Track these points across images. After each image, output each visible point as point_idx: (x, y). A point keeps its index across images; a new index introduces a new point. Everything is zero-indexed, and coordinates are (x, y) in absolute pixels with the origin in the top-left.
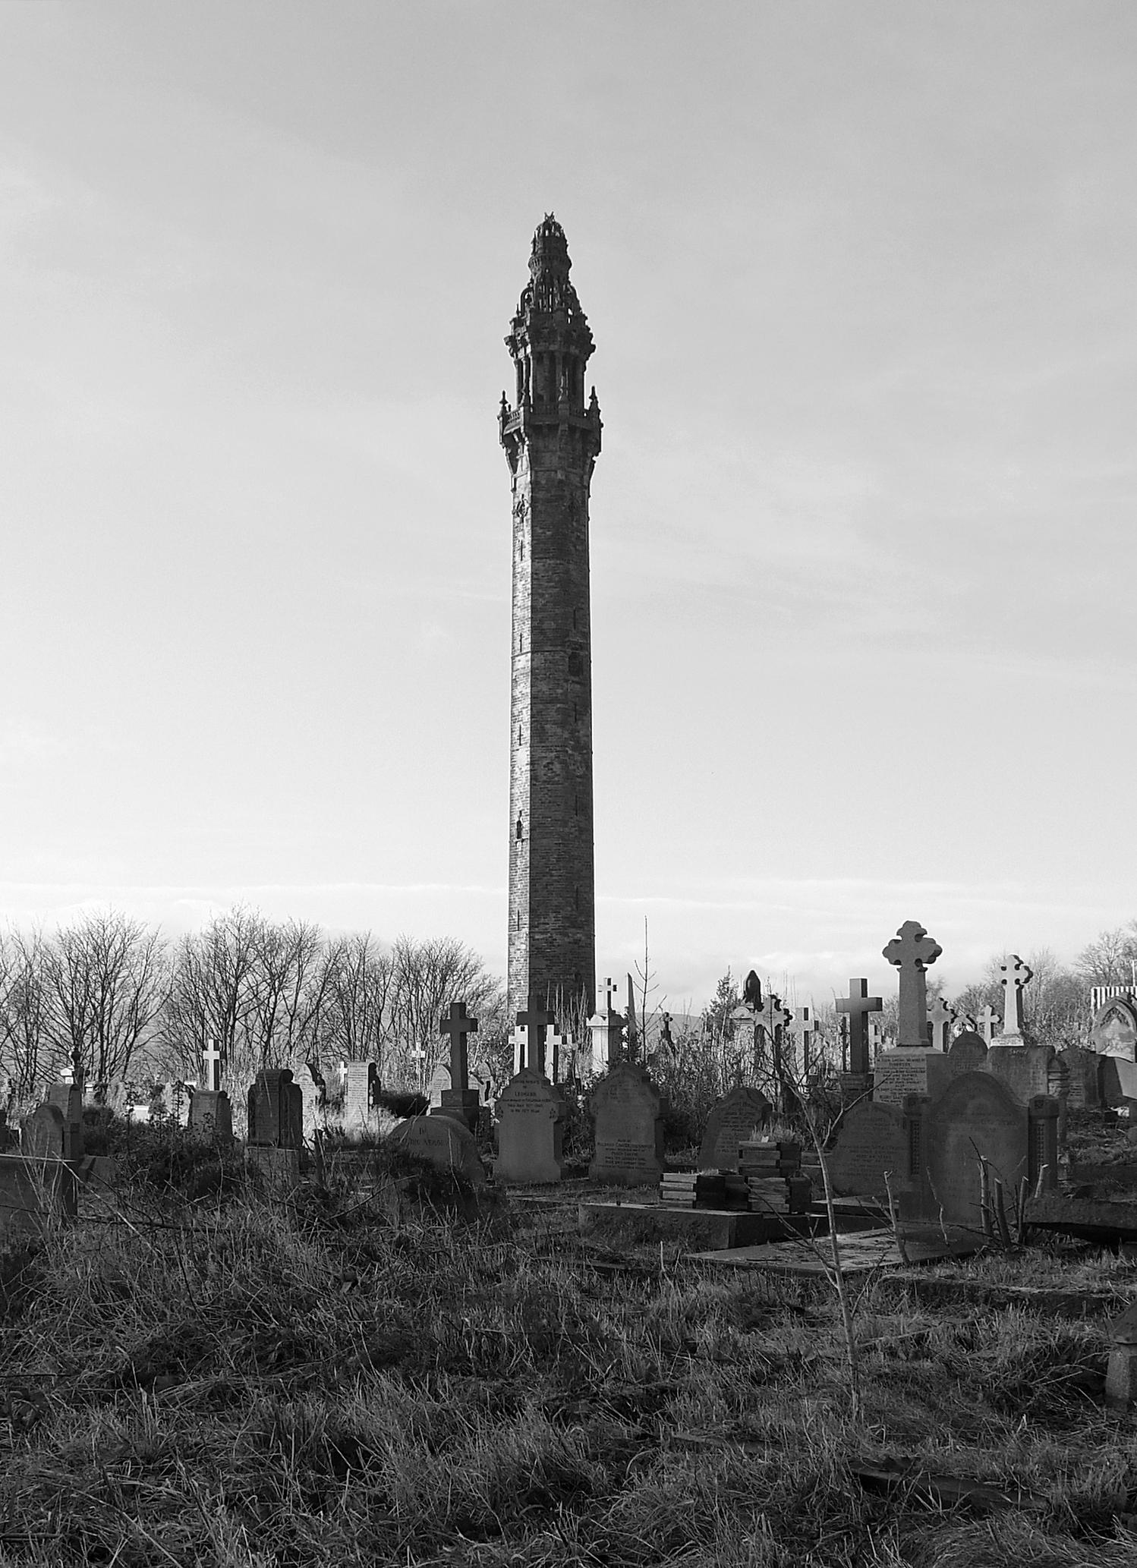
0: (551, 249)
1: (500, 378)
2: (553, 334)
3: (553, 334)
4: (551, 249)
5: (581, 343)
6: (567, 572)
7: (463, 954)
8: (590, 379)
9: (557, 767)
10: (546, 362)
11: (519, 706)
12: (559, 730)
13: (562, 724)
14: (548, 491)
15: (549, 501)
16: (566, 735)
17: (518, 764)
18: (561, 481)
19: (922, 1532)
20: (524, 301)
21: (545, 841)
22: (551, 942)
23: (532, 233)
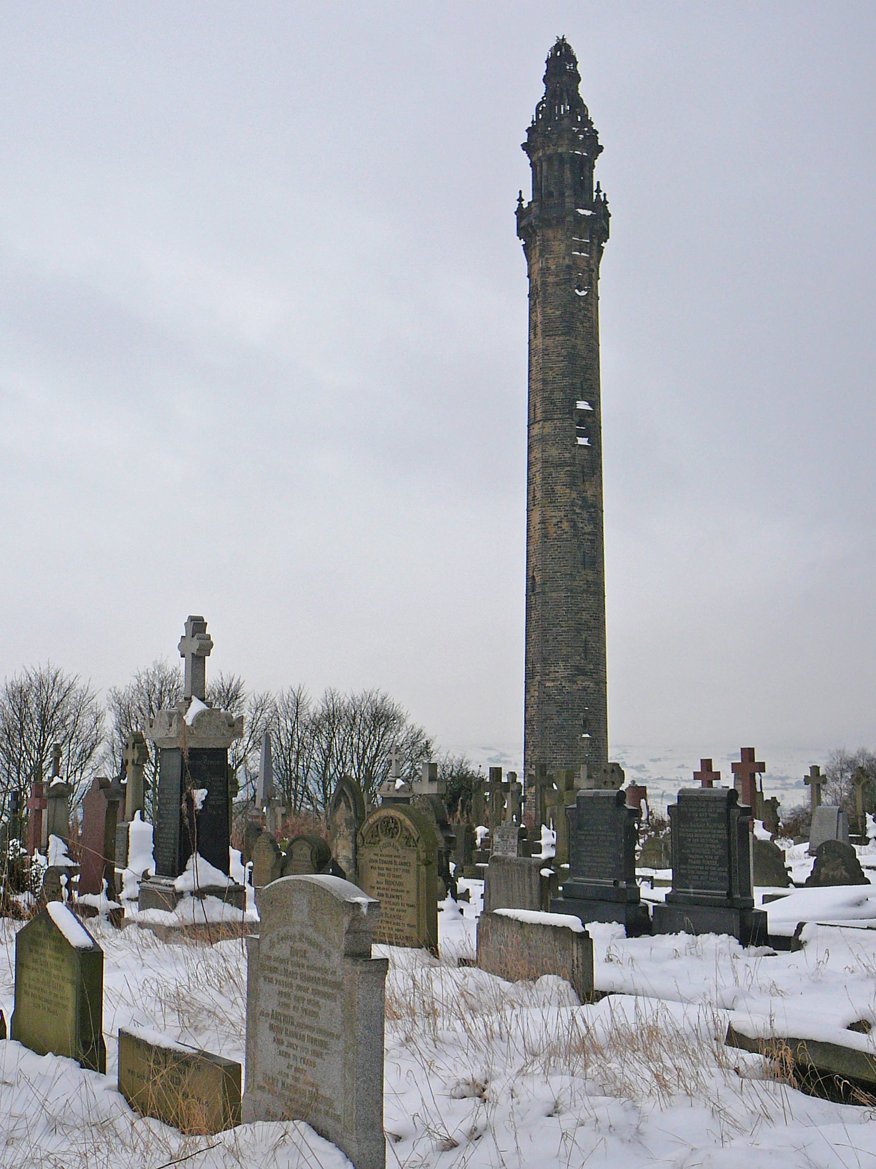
0: (561, 66)
1: (516, 178)
2: (562, 140)
3: (562, 140)
4: (561, 66)
5: (530, 225)
6: (574, 347)
7: (122, 689)
8: (598, 175)
9: (565, 525)
10: (556, 163)
11: (534, 469)
12: (568, 491)
13: (572, 485)
14: (557, 276)
15: (557, 284)
16: (574, 495)
17: (533, 524)
18: (568, 266)
19: (346, 832)
20: (538, 112)
21: (553, 594)
22: (560, 690)
23: (546, 53)
